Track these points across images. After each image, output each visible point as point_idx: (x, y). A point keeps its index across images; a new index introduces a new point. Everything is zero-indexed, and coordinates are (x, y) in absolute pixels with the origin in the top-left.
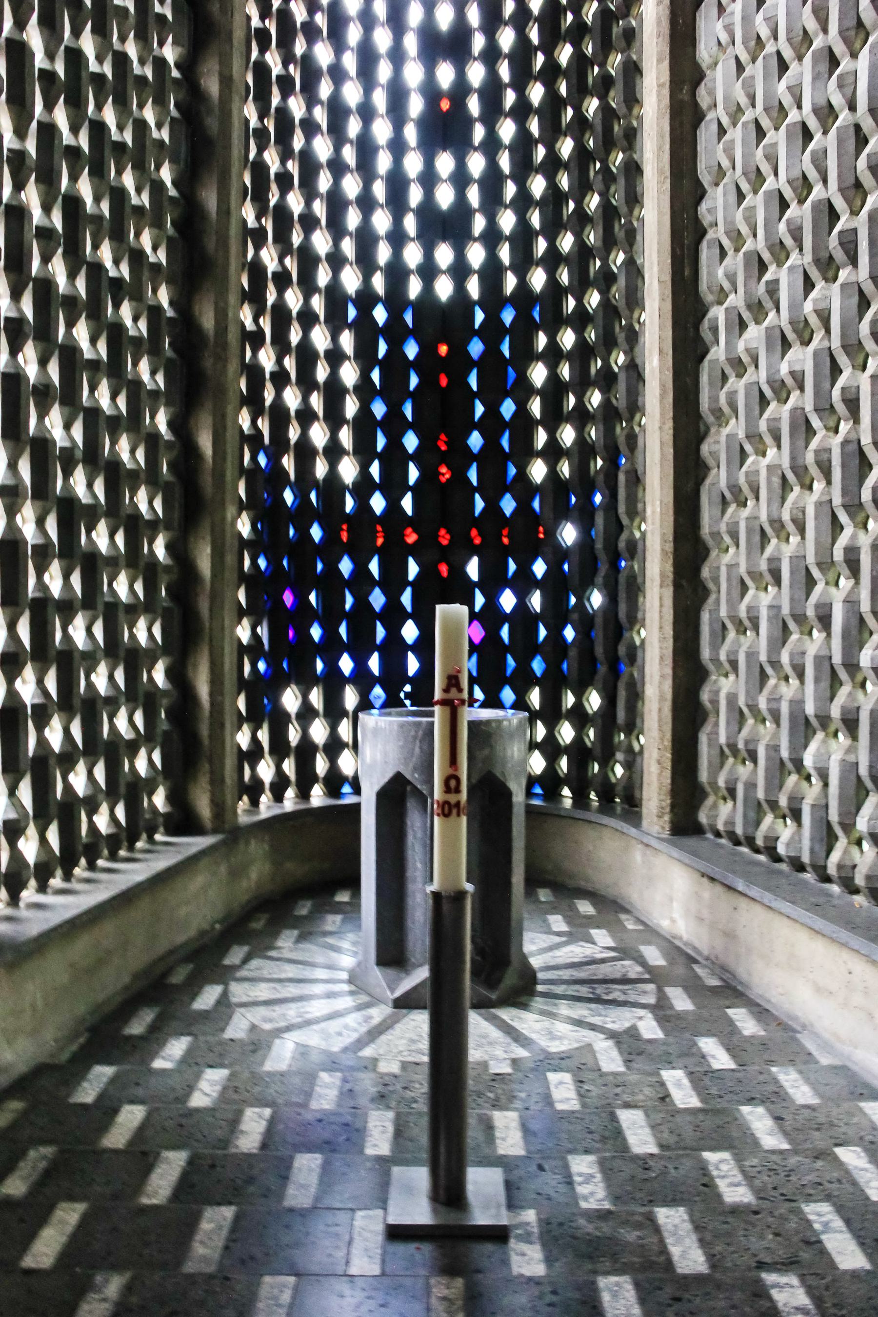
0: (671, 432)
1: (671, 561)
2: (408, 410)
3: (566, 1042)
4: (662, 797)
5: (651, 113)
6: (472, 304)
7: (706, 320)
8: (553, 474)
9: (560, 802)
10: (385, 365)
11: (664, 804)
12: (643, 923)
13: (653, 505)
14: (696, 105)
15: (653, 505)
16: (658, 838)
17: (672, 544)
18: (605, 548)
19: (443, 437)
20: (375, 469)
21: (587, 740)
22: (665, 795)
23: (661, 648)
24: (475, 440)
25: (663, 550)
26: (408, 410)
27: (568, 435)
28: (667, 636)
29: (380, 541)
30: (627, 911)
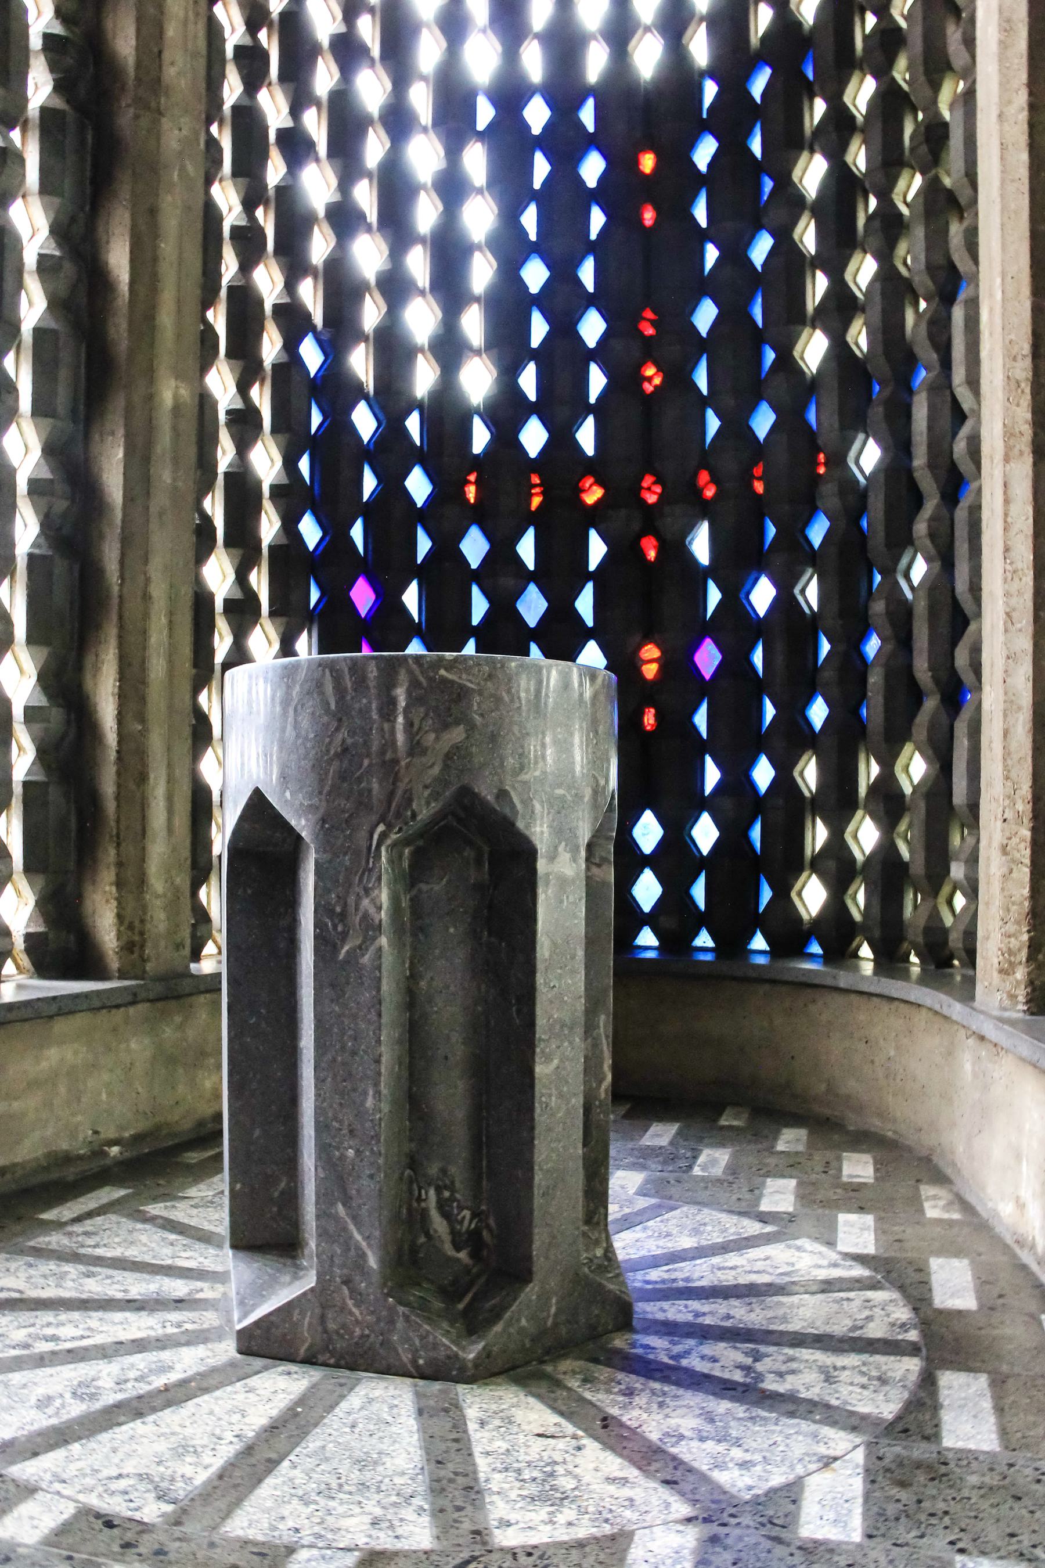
0: (1024, 116)
1: (1026, 400)
3: (568, 1513)
4: (1011, 928)
8: (840, 349)
9: (856, 969)
11: (1014, 943)
12: (966, 1207)
16: (1001, 1020)
17: (1028, 362)
18: (932, 465)
20: (528, 381)
22: (1018, 923)
23: (1007, 594)
28: (1020, 565)
29: (536, 501)
30: (940, 1178)
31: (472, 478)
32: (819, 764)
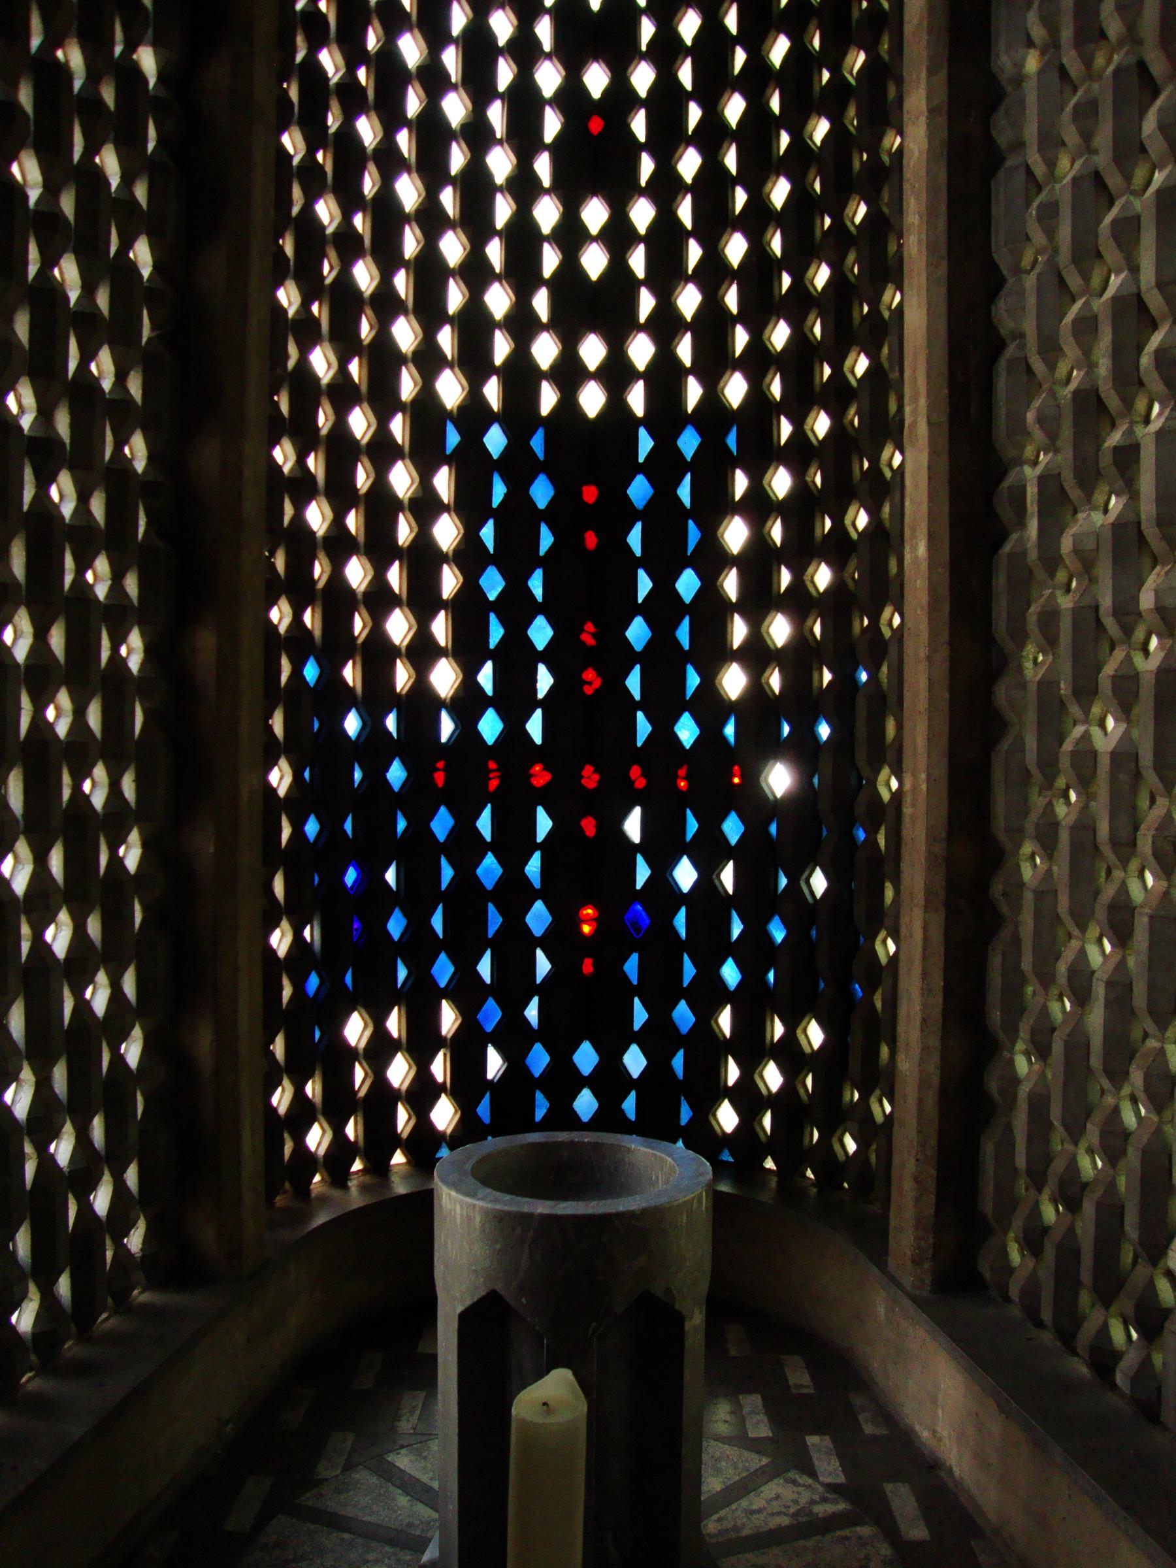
2: (536, 584)
5: (917, 154)
6: (636, 422)
7: (1006, 484)
8: (757, 687)
10: (502, 516)
13: (914, 776)
14: (990, 141)
15: (914, 776)
19: (589, 627)
20: (486, 677)
21: (802, 1091)
24: (638, 632)
25: (929, 852)
26: (536, 584)
27: (780, 630)
29: (493, 784)
31: (440, 765)
32: (395, 539)
